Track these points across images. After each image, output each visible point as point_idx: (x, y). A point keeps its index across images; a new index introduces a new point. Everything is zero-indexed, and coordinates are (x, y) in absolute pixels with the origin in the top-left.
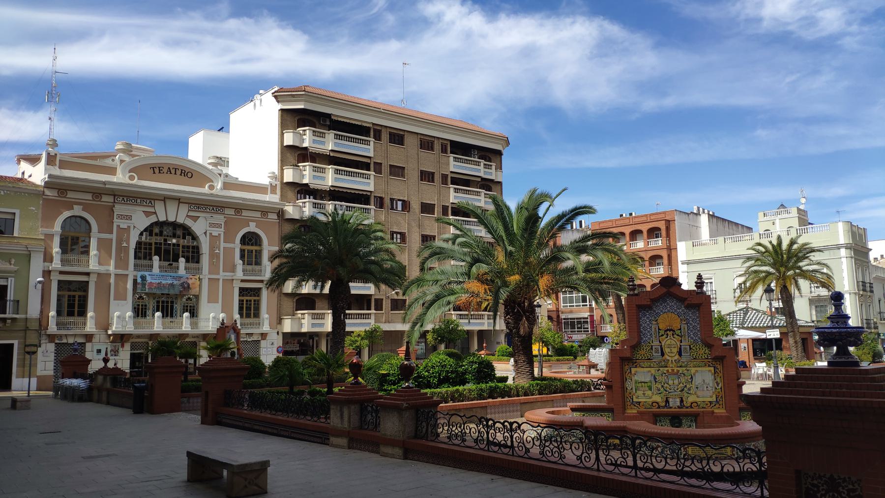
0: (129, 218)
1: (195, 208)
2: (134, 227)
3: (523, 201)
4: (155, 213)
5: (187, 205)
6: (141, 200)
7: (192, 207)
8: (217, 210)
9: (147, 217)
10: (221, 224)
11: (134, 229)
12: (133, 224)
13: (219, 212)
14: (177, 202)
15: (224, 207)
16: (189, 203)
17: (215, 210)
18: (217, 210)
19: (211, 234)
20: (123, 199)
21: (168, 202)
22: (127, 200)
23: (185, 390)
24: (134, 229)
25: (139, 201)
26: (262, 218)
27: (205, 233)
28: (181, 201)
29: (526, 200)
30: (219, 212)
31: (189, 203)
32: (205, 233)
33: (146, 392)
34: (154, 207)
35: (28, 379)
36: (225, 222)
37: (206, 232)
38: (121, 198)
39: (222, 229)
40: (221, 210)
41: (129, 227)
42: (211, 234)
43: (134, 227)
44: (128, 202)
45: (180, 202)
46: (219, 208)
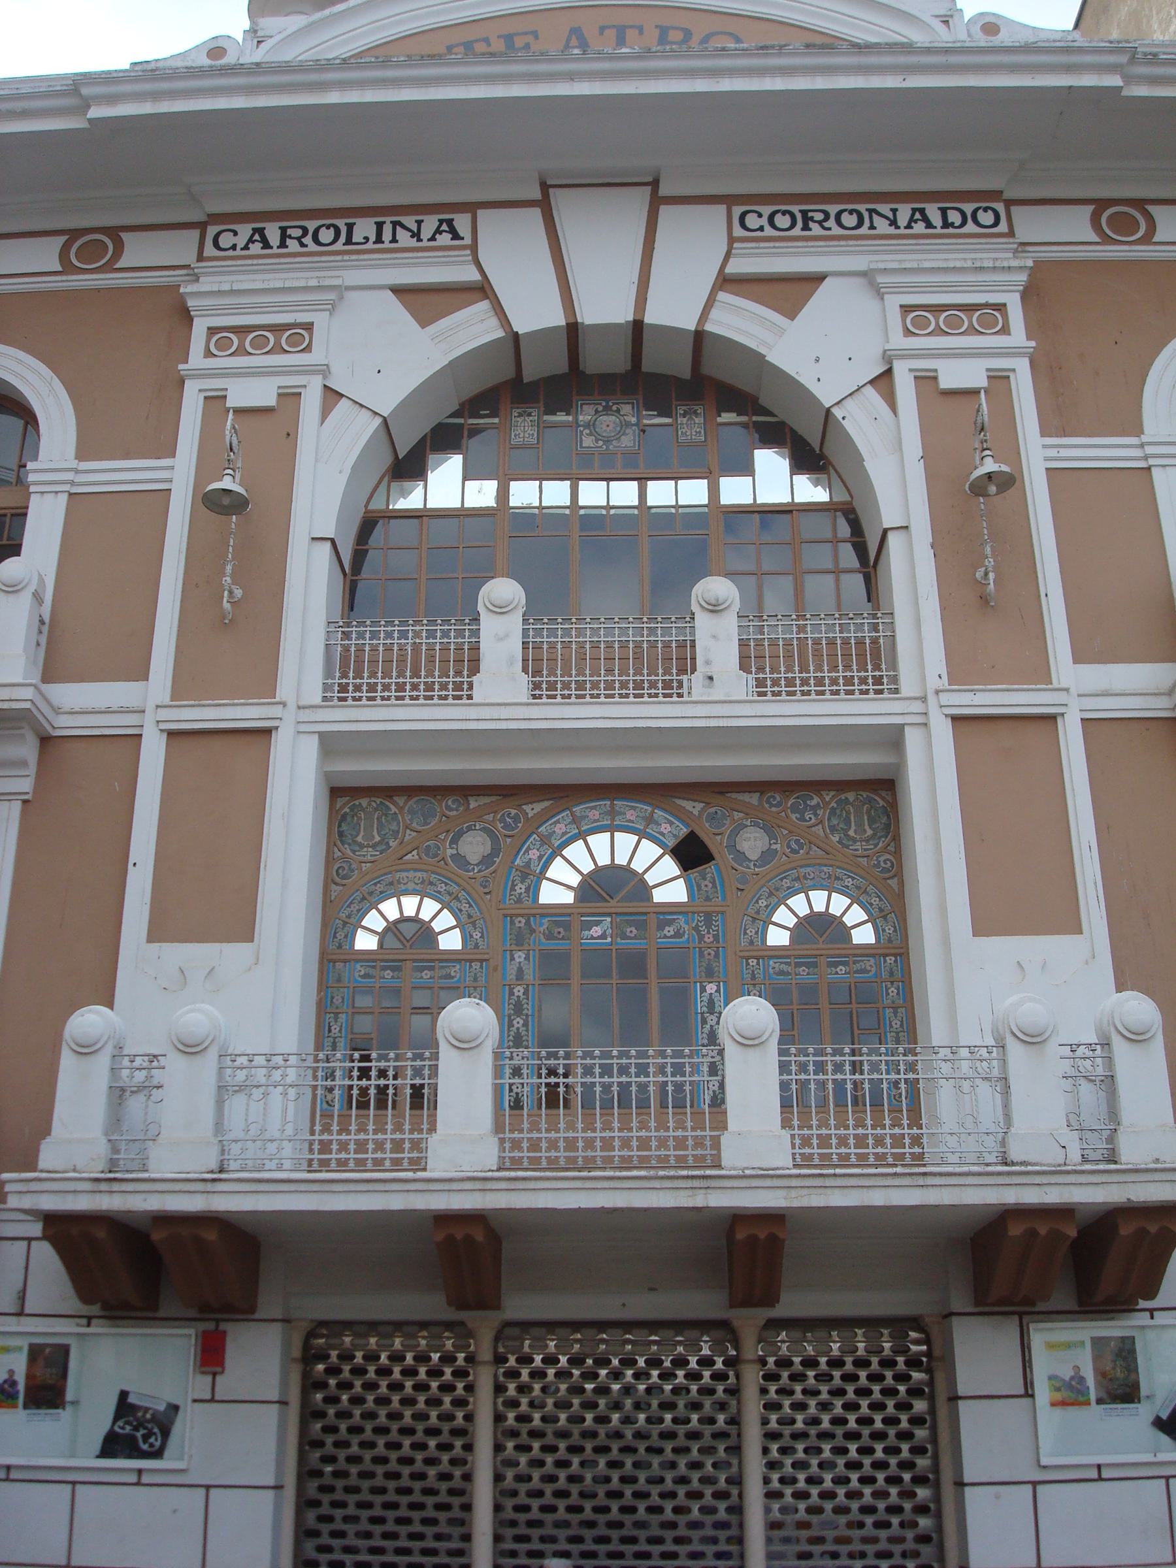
0: (295, 341)
1: (783, 221)
2: (332, 396)
3: (916, 43)
4: (483, 290)
5: (722, 208)
6: (380, 226)
7: (752, 221)
8: (955, 217)
9: (424, 321)
10: (1001, 308)
11: (325, 412)
12: (324, 371)
13: (971, 227)
14: (637, 201)
15: (472, 208)
16: (728, 200)
17: (936, 219)
18: (955, 217)
19: (926, 381)
20: (261, 231)
21: (561, 200)
22: (284, 236)
23: (361, 1048)
24: (325, 412)
25: (364, 228)
26: (67, 268)
27: (884, 381)
28: (664, 191)
29: (919, 45)
30: (971, 227)
31: (728, 200)
32: (884, 381)
33: (913, 1335)
34: (474, 248)
35: (280, 1317)
36: (1028, 295)
37: (889, 372)
38: (245, 231)
39: (1018, 336)
40: (986, 218)
41: (290, 398)
42: (926, 381)
43: (332, 396)
44: (816, 230)
45: (657, 202)
46: (968, 208)
